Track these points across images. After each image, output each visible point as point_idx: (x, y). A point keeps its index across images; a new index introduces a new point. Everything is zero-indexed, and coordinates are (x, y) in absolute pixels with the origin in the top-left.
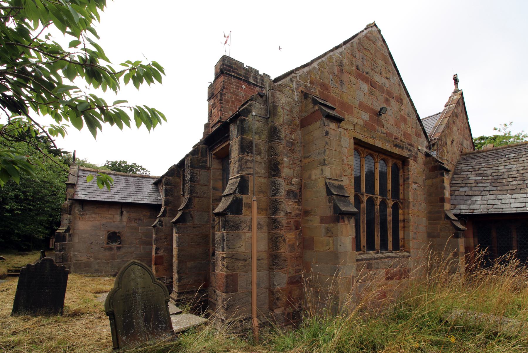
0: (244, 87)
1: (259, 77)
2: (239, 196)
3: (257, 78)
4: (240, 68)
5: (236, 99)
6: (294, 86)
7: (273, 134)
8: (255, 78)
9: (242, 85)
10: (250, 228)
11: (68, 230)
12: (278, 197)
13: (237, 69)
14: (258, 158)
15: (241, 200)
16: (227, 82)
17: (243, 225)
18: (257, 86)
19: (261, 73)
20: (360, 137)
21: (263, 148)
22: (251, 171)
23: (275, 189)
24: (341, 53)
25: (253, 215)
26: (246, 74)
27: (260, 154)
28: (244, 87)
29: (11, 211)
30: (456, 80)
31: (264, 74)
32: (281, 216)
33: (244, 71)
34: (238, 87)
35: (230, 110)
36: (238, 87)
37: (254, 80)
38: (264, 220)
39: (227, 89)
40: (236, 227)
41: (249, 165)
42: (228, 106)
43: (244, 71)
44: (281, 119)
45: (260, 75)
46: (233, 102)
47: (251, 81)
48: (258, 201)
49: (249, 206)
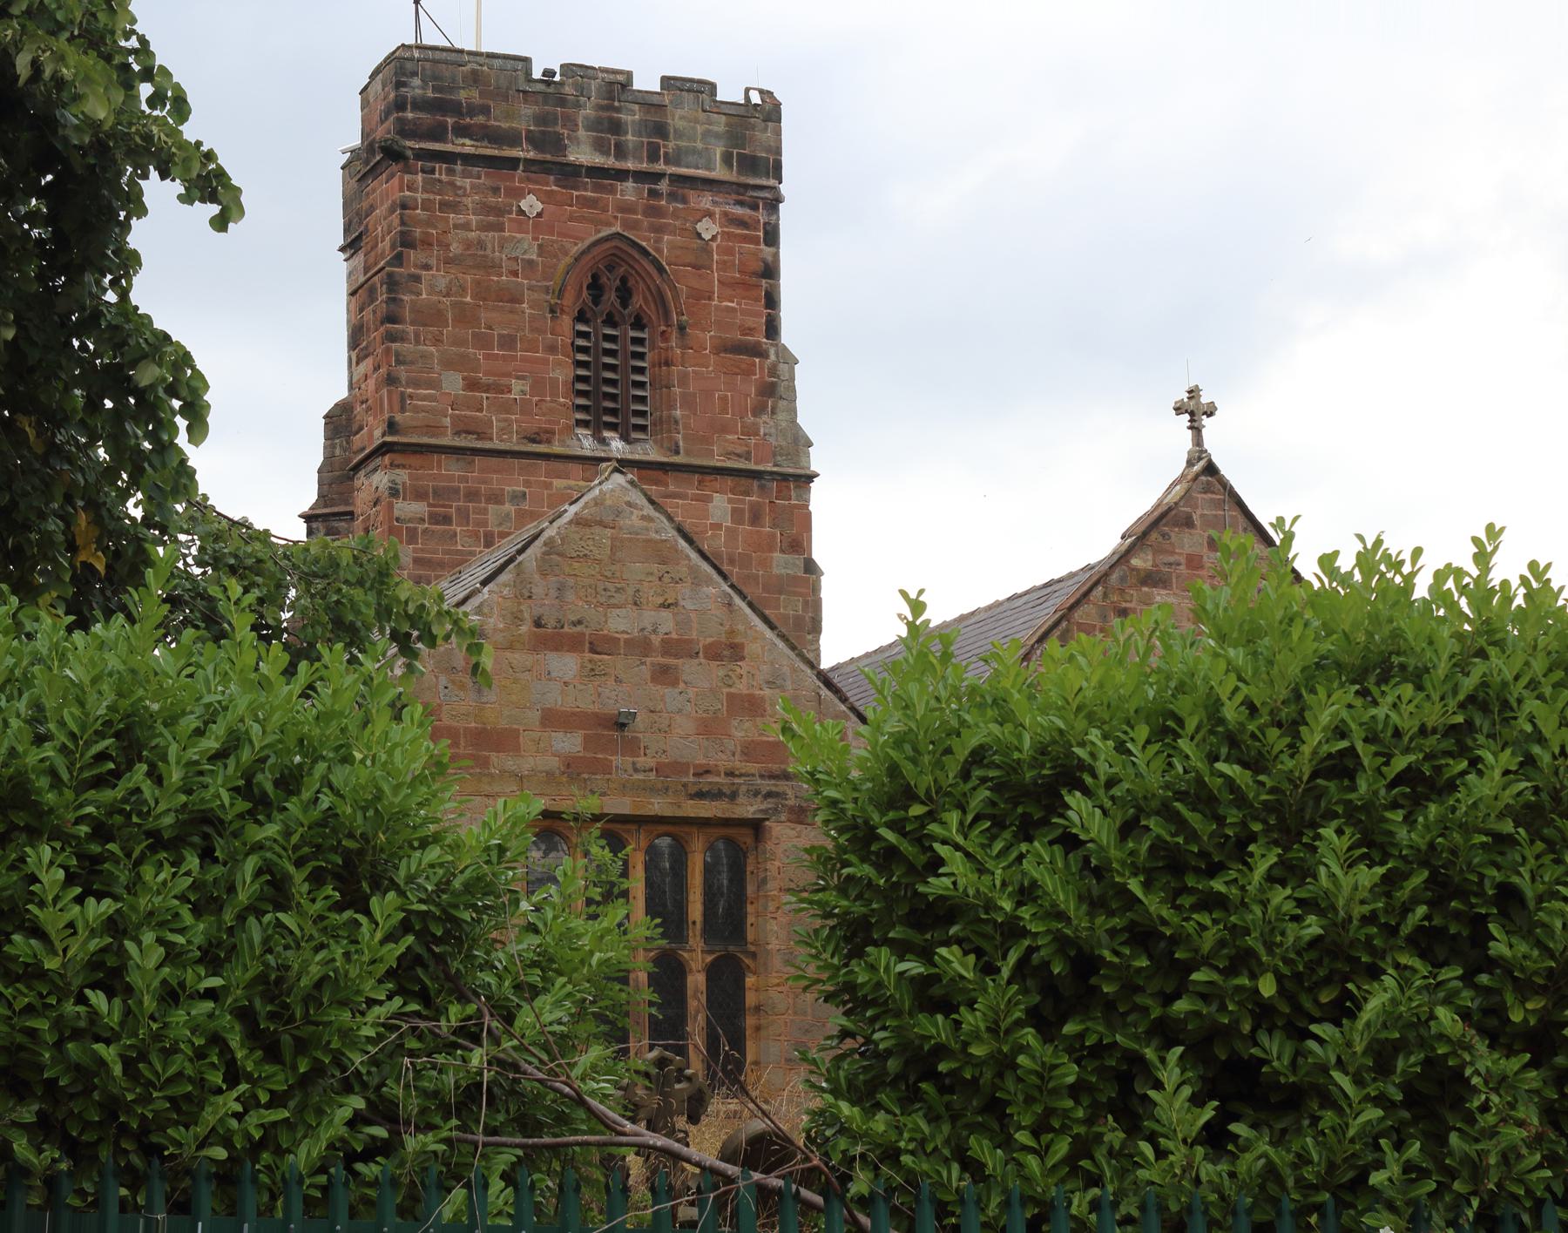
1: (631, 117)
3: (616, 127)
5: (482, 292)
9: (520, 194)
13: (485, 110)
16: (427, 205)
18: (622, 175)
19: (646, 81)
26: (541, 119)
31: (666, 81)
33: (528, 110)
34: (494, 217)
35: (449, 364)
37: (600, 146)
39: (427, 243)
42: (437, 341)
43: (528, 110)
45: (647, 102)
46: (465, 316)
47: (582, 154)
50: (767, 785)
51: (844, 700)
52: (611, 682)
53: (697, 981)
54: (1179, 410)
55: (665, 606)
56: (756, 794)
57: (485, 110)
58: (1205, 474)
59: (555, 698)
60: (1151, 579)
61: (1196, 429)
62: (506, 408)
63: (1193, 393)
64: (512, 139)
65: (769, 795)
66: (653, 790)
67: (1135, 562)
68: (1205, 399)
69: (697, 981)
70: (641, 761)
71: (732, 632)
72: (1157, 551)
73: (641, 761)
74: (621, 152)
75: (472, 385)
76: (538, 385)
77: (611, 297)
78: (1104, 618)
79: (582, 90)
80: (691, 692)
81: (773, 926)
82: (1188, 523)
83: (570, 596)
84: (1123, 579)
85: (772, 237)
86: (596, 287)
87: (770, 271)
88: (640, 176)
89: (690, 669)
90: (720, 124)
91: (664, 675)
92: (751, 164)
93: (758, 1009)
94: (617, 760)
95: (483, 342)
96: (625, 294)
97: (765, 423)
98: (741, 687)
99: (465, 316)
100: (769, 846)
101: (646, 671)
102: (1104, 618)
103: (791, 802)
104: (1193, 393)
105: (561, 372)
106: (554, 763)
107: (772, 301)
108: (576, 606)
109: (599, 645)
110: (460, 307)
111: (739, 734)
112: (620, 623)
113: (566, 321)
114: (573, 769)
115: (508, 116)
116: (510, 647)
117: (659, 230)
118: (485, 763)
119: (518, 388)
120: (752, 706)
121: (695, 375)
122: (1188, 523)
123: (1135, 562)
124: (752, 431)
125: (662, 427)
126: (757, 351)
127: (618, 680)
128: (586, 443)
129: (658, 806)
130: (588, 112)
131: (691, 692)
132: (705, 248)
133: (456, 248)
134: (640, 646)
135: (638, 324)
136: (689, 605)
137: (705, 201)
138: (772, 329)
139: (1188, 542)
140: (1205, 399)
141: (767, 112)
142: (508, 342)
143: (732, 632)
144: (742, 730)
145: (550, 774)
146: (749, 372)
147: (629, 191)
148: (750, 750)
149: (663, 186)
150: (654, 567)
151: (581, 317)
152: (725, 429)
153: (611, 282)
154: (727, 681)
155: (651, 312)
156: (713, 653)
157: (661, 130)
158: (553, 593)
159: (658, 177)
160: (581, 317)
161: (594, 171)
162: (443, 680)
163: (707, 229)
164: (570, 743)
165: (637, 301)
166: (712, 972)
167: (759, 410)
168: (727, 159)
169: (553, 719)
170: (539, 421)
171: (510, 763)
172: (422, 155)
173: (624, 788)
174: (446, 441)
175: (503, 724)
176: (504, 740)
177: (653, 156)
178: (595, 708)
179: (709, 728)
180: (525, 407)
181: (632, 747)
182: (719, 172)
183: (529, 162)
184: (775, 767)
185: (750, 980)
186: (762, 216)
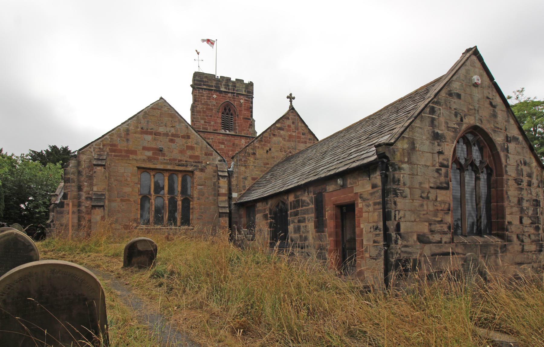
0: (215, 96)
1: (230, 84)
2: (63, 200)
3: (228, 86)
4: (210, 80)
5: (207, 109)
6: (92, 150)
7: (79, 173)
8: (227, 86)
9: (213, 95)
10: (68, 213)
11: (52, 221)
12: (81, 200)
13: (208, 82)
14: (73, 184)
15: (64, 202)
16: (199, 95)
17: (65, 212)
18: (229, 93)
19: (233, 79)
20: (138, 166)
21: (76, 180)
22: (69, 190)
23: (79, 197)
24: (128, 125)
25: (70, 207)
26: (216, 84)
27: (74, 182)
28: (215, 96)
29: (40, 212)
30: (291, 98)
31: (236, 79)
32: (83, 208)
33: (215, 82)
34: (209, 98)
35: (202, 119)
36: (209, 98)
37: (226, 88)
38: (76, 209)
39: (198, 101)
40: (61, 213)
41: (68, 188)
42: (200, 115)
43: (215, 82)
44: (83, 167)
45: (233, 82)
46: (204, 112)
47: (223, 89)
48: (73, 202)
49: (68, 205)
50: (194, 164)
51: (212, 148)
52: (159, 142)
53: (179, 203)
54: (288, 97)
55: (172, 127)
56: (192, 165)
57: (208, 82)
58: (292, 109)
59: (146, 144)
60: (280, 129)
61: (291, 101)
62: (210, 126)
63: (291, 94)
64: (212, 86)
65: (195, 166)
66: (168, 164)
67: (277, 125)
68: (293, 96)
69: (179, 203)
70: (166, 158)
71: (188, 133)
72: (282, 123)
73: (166, 158)
74: (229, 89)
75: (205, 122)
76: (215, 123)
77: (227, 111)
78: (270, 135)
79: (223, 80)
80: (178, 145)
81: (195, 192)
82: (288, 119)
83: (150, 123)
84: (274, 128)
85: (252, 103)
86: (225, 109)
87: (252, 108)
88: (232, 93)
89: (177, 140)
90: (244, 86)
91: (172, 141)
92: (249, 92)
93: (192, 208)
94: (160, 158)
95: (207, 116)
96: (230, 110)
97: (250, 130)
98: (189, 144)
99: (204, 112)
100: (195, 176)
101: (167, 140)
102: (270, 135)
103: (200, 168)
104: (291, 94)
105: (219, 121)
106: (145, 157)
107: (252, 112)
108: (151, 126)
109: (157, 134)
110: (203, 111)
111: (189, 154)
112: (162, 130)
113: (220, 114)
114: (149, 159)
115: (211, 83)
116: (135, 133)
117: (234, 101)
118: (129, 157)
119: (212, 123)
120: (192, 148)
121: (239, 121)
122: (288, 119)
123: (277, 125)
124: (248, 131)
125: (235, 130)
126: (249, 119)
127: (161, 141)
128: (223, 131)
129: (169, 167)
130: (224, 83)
131: (178, 145)
132: (242, 104)
133: (203, 102)
134: (166, 135)
135: (232, 115)
136: (178, 127)
137: (242, 97)
138: (252, 116)
139: (289, 122)
140: (293, 96)
141: (251, 84)
142: (211, 116)
143: (188, 133)
144: (189, 153)
145: (144, 160)
146: (248, 122)
147: (230, 95)
148: (191, 157)
149: (235, 94)
150: (170, 119)
151: (223, 113)
152: (244, 130)
153: (227, 109)
154: (186, 143)
155: (233, 113)
156: (183, 137)
157: (235, 86)
158: (146, 122)
159: (234, 93)
160: (223, 113)
161: (224, 92)
162: (119, 139)
163: (242, 101)
164: (150, 154)
165: (231, 111)
166: (183, 201)
167: (249, 128)
168: (245, 91)
169: (145, 148)
170: (216, 128)
171: (135, 157)
172: (198, 88)
173: (161, 163)
174: (201, 130)
175: (133, 149)
176: (134, 152)
177: (234, 90)
178: (156, 147)
179: (182, 152)
180: (214, 126)
181: (164, 155)
182: (244, 93)
183: (215, 90)
184: (196, 160)
185: (191, 203)
186: (250, 100)
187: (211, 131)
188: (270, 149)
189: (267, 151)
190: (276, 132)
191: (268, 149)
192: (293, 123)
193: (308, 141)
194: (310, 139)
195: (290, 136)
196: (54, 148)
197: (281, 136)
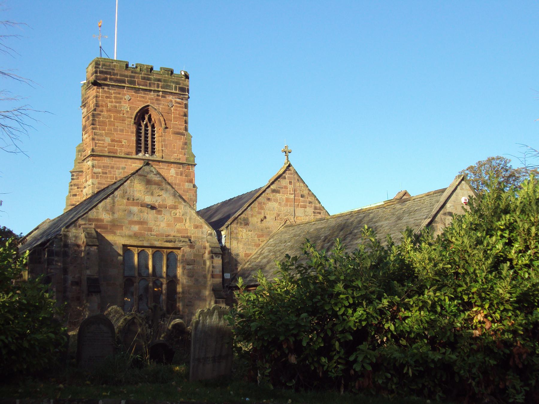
65: (184, 242)
75: (113, 141)
117: (159, 104)
149: (161, 93)
159: (159, 91)
187: (123, 155)
188: (265, 217)
189: (262, 220)
190: (271, 196)
191: (262, 216)
192: (290, 183)
193: (308, 204)
194: (310, 203)
195: (287, 200)
196: (5, 228)
197: (276, 200)
